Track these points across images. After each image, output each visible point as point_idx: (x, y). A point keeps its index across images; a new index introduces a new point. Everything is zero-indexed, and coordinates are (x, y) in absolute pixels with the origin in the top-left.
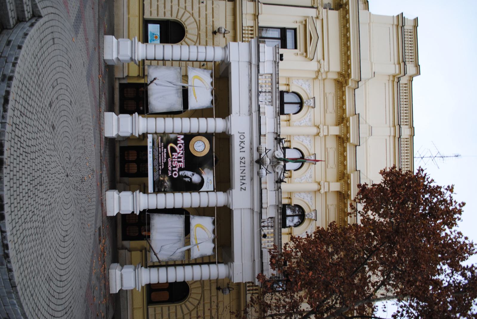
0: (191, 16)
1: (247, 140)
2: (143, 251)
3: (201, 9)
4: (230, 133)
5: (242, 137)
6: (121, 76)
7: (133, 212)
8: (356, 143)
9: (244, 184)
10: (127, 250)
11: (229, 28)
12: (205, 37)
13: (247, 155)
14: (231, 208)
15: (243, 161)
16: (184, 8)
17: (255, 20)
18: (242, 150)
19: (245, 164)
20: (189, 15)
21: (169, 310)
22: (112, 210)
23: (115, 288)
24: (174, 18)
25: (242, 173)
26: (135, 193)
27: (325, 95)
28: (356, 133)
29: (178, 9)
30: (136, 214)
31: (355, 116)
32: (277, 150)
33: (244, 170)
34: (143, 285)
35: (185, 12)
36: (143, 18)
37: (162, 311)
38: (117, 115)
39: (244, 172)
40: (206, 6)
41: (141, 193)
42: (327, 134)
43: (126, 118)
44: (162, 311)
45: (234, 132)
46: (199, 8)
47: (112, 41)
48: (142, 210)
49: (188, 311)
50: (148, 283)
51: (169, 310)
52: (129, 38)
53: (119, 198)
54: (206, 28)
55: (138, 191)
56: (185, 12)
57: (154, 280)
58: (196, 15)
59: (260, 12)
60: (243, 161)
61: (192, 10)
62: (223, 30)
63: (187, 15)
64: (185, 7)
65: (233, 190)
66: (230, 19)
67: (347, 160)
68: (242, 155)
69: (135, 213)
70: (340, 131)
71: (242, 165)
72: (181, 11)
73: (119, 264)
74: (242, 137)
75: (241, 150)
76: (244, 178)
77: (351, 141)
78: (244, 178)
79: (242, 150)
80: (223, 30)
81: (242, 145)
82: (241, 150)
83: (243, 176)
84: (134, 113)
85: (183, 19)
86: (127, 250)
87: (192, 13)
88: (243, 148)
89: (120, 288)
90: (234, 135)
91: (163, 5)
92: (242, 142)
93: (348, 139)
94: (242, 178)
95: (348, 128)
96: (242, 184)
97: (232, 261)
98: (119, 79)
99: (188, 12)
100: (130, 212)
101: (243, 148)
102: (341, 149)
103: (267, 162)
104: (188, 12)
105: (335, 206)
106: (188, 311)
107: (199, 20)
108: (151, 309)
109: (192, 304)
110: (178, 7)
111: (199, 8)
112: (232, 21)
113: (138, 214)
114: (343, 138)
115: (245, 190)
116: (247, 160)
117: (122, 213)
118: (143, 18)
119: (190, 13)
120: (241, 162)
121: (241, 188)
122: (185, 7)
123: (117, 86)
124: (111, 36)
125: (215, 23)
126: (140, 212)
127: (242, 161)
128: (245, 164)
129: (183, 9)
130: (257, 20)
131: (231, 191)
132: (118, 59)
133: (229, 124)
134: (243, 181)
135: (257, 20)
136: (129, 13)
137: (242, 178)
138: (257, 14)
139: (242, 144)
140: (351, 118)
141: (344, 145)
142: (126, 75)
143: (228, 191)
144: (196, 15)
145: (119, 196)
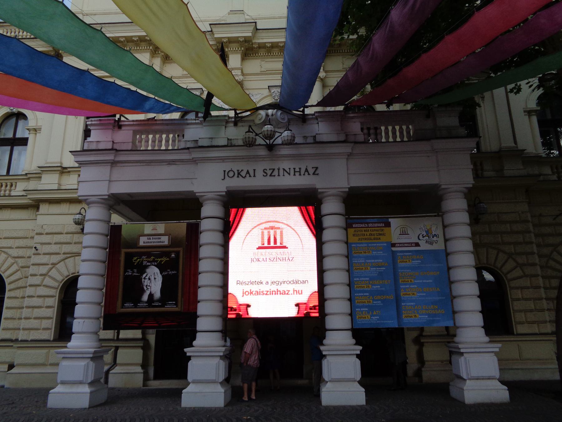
0: (57, 266)
1: (236, 166)
2: (422, 341)
3: (47, 251)
4: (224, 193)
5: (231, 174)
6: (141, 377)
7: (358, 356)
8: (252, 28)
9: (306, 170)
10: (423, 369)
11: (75, 208)
12: (62, 235)
13: (260, 167)
14: (347, 190)
15: (269, 172)
16: (43, 277)
17: (69, 172)
18: (252, 173)
19: (274, 170)
20: (54, 269)
21: (518, 300)
22: (356, 396)
23: (501, 394)
24: (56, 293)
25: (289, 174)
26: (324, 353)
27: (262, 73)
28: (239, 29)
29: (44, 286)
30: (361, 351)
31: (214, 30)
32: (254, 121)
33: (284, 169)
34: (487, 339)
35: (50, 277)
36: (55, 340)
37: (521, 311)
38: (188, 384)
39: (288, 171)
40: (42, 244)
41: (325, 342)
42: (240, 71)
43: (195, 369)
44: (521, 311)
45: (222, 187)
46: (44, 254)
47: (59, 393)
48: (354, 341)
49: (518, 268)
50: (483, 330)
51: (518, 300)
52: (57, 364)
53: (63, 383)
54: (75, 243)
55: (322, 348)
56: (50, 277)
57: (478, 319)
58: (55, 259)
59: (59, 165)
60: (269, 172)
61: (48, 264)
62: (78, 217)
63: (53, 273)
64: (41, 275)
65: (317, 187)
66: (64, 208)
67: (278, 42)
68: (260, 173)
69: (359, 352)
70: (235, 52)
71: (276, 173)
72: (48, 281)
73: (451, 383)
74: (231, 174)
75: (252, 174)
76: (297, 170)
77: (250, 34)
78: (297, 170)
79: (252, 173)
80: (78, 217)
81: (243, 174)
82: (252, 174)
83: (295, 172)
84: (186, 353)
85: (60, 278)
86: (423, 369)
87: (52, 264)
88: (248, 172)
89: (497, 381)
90: (227, 187)
91: (36, 310)
92: (239, 174)
93: (247, 40)
94: (297, 174)
95: (231, 41)
96: (306, 173)
97: (436, 187)
98: (146, 379)
99: (49, 271)
100: (358, 362)
101: (248, 172)
102: (262, 52)
103: (270, 129)
104: (49, 271)
105: (344, 59)
106: (518, 268)
107: (64, 254)
108: (521, 329)
109: (506, 261)
110: (42, 287)
111: (44, 254)
112: (68, 204)
113: (361, 348)
114: (247, 49)
115: (317, 168)
116: (267, 165)
117: (359, 376)
118: (55, 340)
119: (51, 269)
120: (271, 175)
121: (314, 174)
122: (41, 275)
123: (155, 384)
124: (50, 396)
125: (70, 231)
126: (356, 344)
127: (269, 174)
128: (274, 170)
129: (44, 278)
130: (69, 170)
131: (319, 191)
132: (91, 384)
133: (210, 195)
134: (303, 171)
135: (69, 170)
136: (44, 365)
137: (297, 174)
138: (60, 169)
139: (242, 174)
140: (216, 36)
141: (256, 46)
142: (140, 368)
143: (319, 196)
144: (55, 259)
145: (330, 381)
